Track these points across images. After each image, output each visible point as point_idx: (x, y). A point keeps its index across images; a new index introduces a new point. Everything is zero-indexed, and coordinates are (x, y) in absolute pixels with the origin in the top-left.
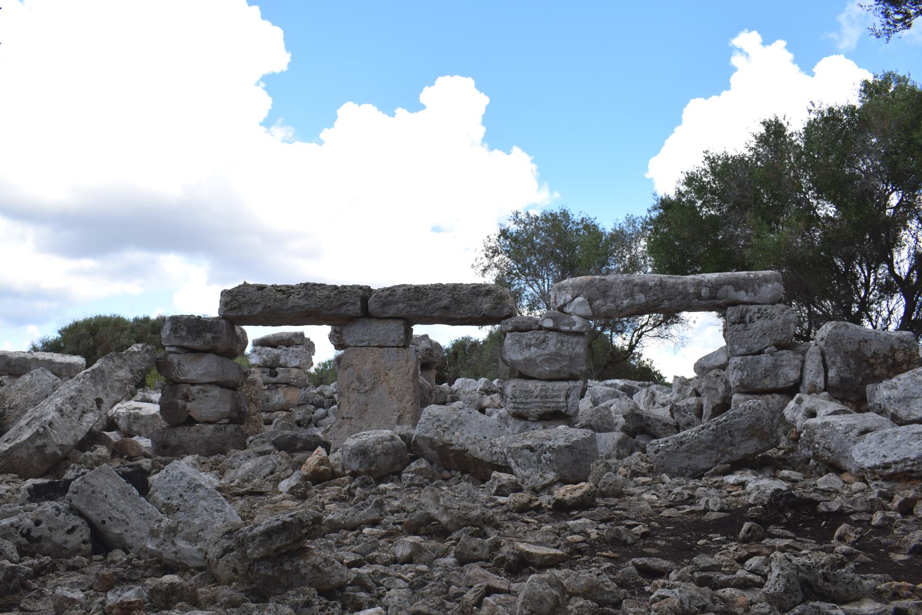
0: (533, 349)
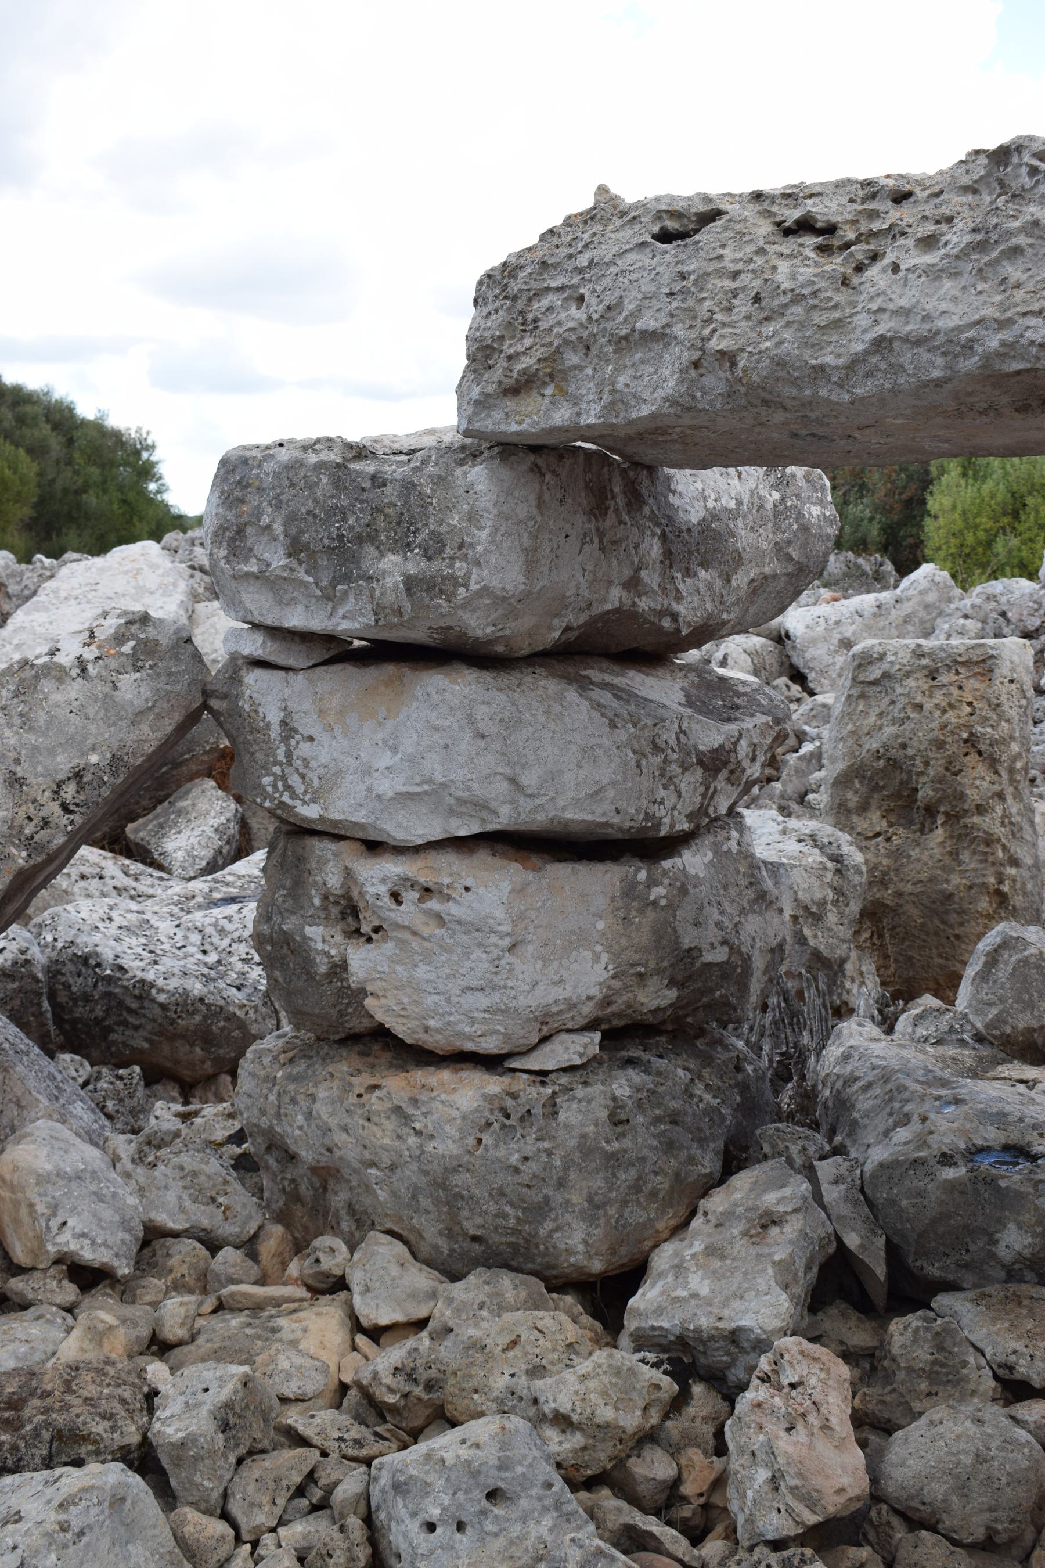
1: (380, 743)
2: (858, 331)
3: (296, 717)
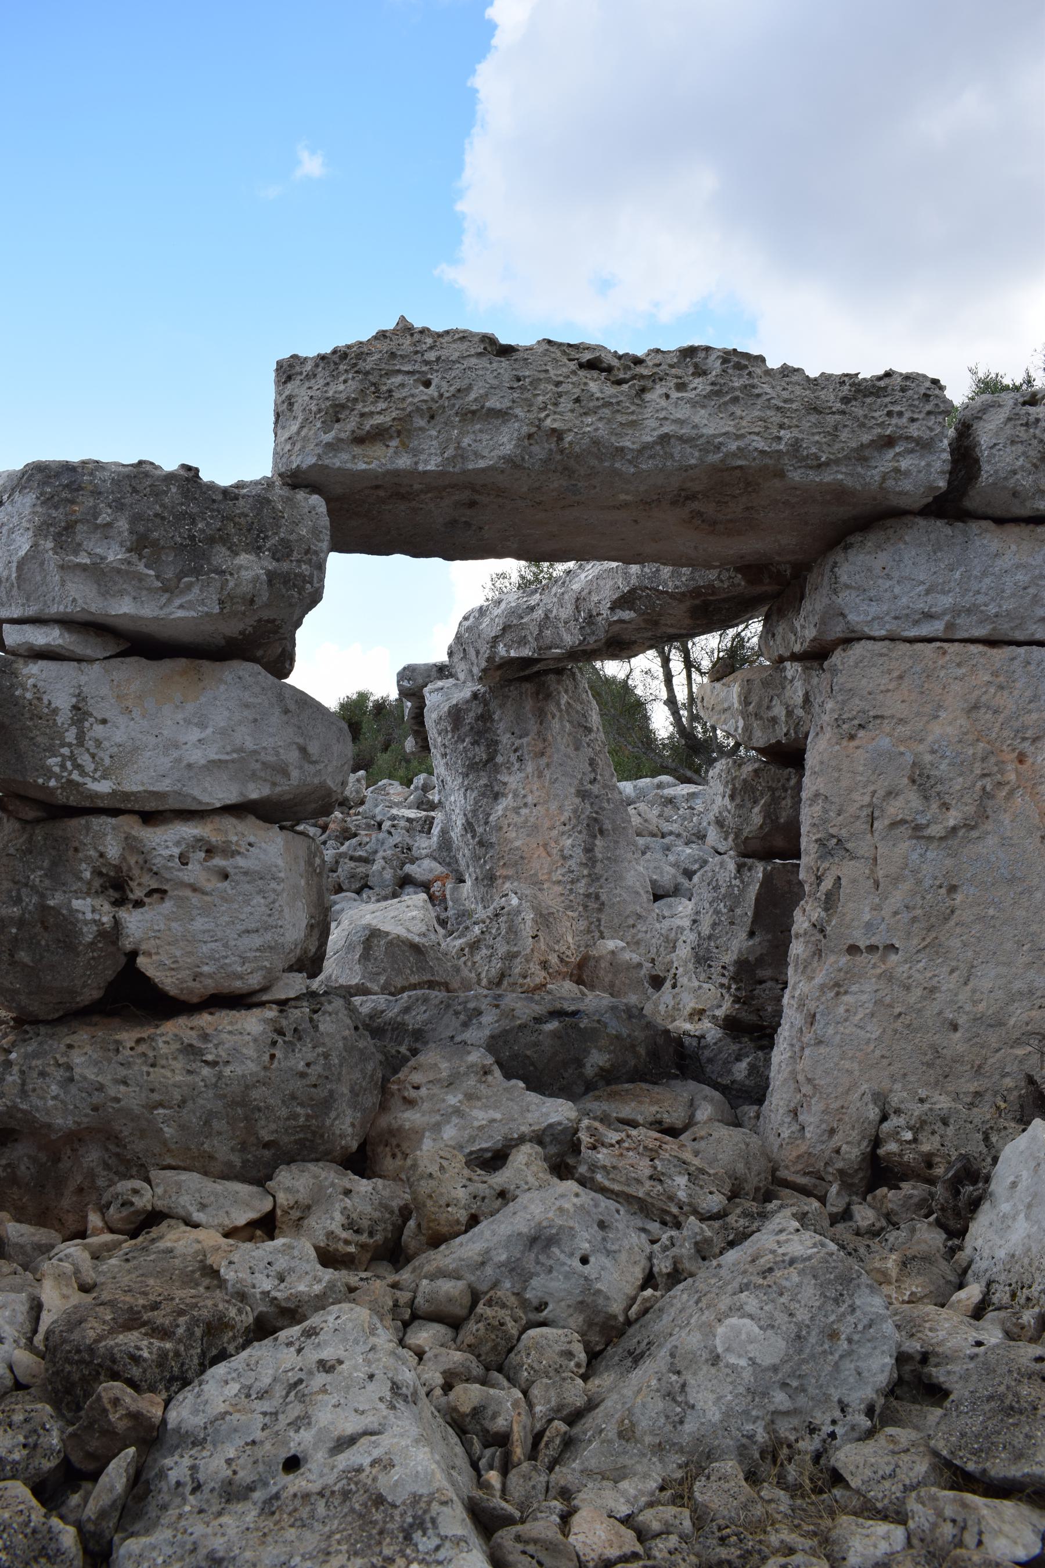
1: (182, 722)
2: (648, 430)
3: (90, 702)
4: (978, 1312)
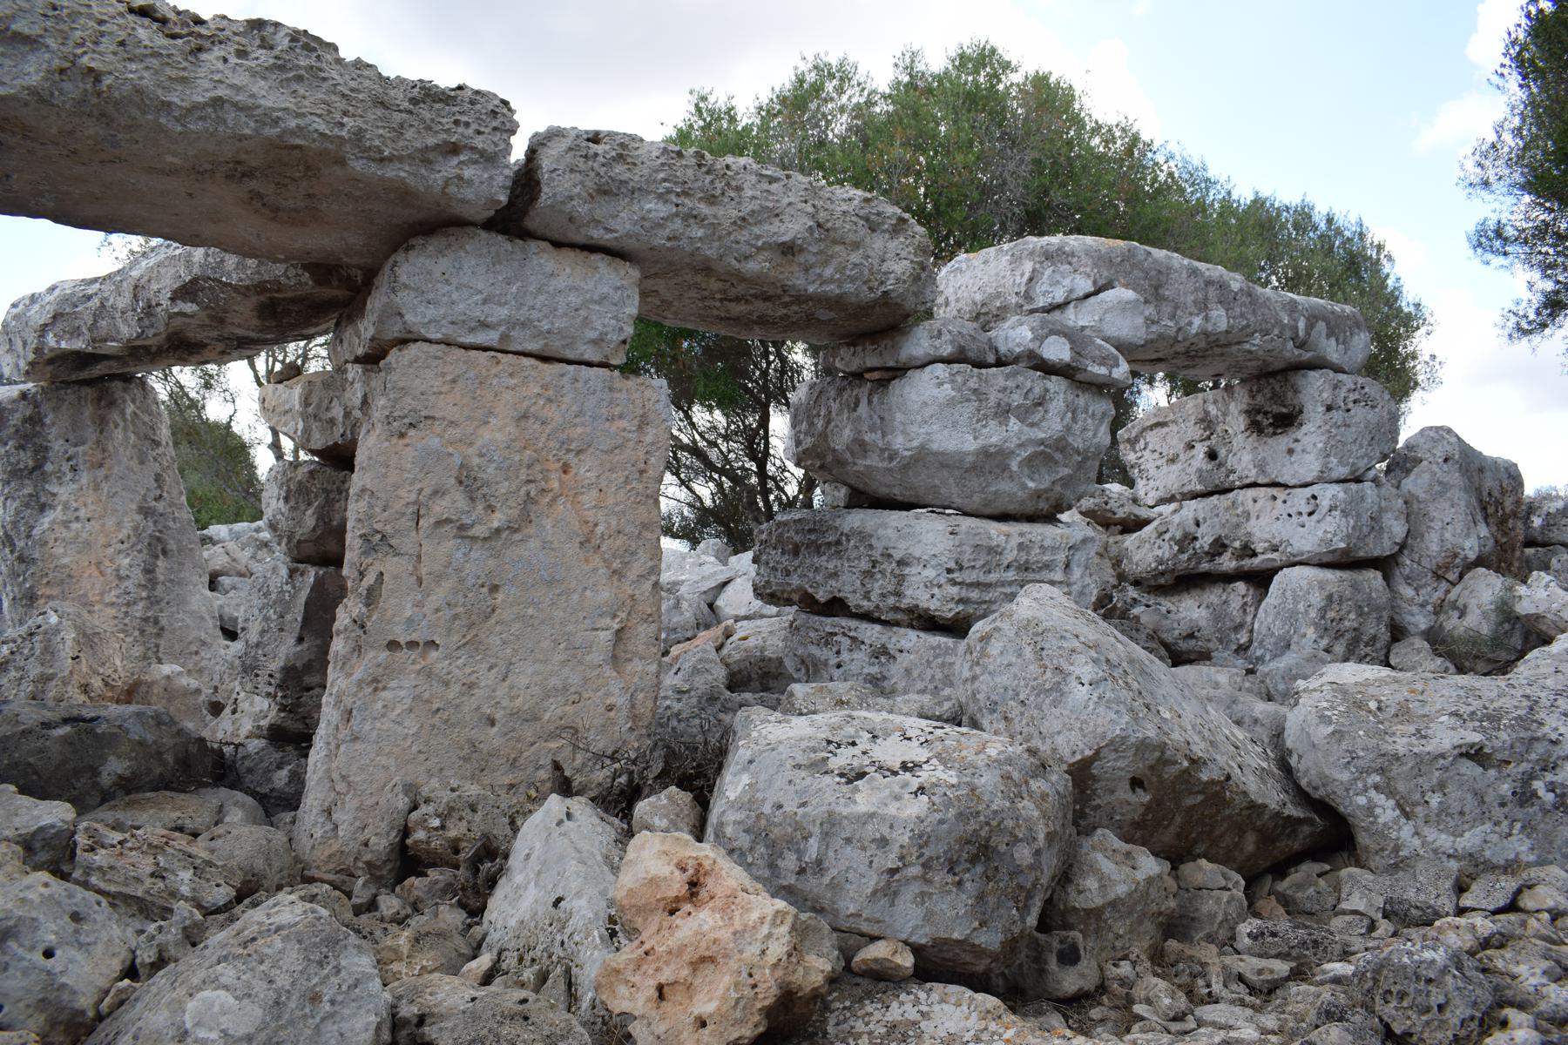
0: (1014, 424)
4: (487, 979)
